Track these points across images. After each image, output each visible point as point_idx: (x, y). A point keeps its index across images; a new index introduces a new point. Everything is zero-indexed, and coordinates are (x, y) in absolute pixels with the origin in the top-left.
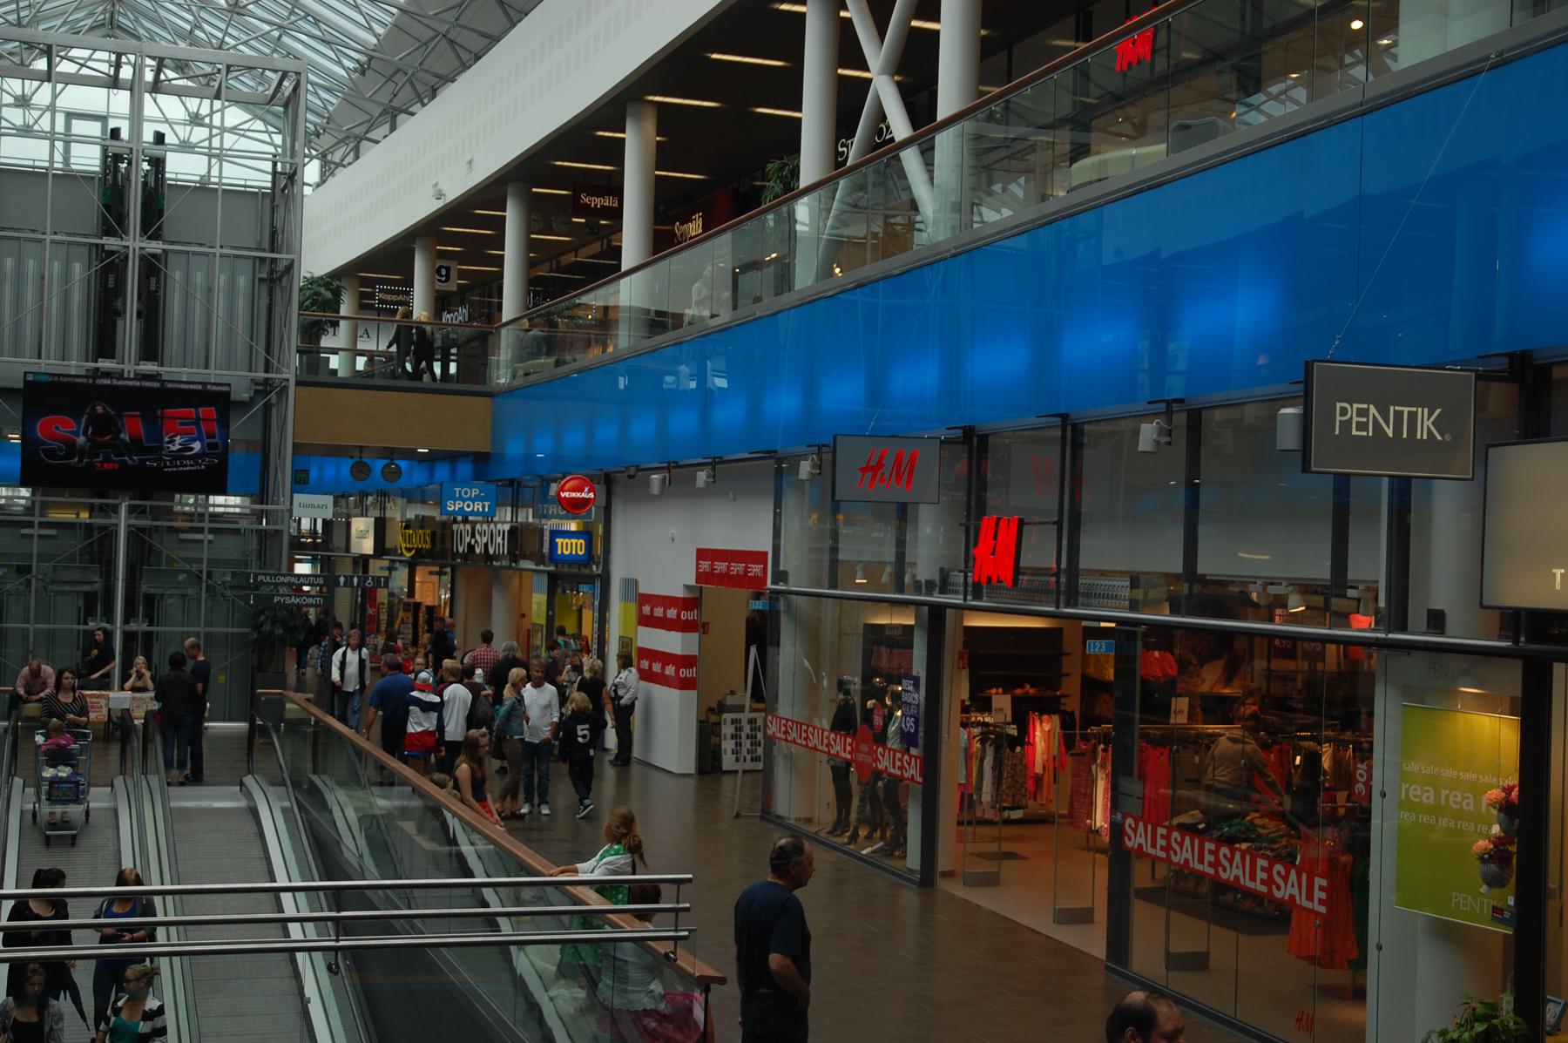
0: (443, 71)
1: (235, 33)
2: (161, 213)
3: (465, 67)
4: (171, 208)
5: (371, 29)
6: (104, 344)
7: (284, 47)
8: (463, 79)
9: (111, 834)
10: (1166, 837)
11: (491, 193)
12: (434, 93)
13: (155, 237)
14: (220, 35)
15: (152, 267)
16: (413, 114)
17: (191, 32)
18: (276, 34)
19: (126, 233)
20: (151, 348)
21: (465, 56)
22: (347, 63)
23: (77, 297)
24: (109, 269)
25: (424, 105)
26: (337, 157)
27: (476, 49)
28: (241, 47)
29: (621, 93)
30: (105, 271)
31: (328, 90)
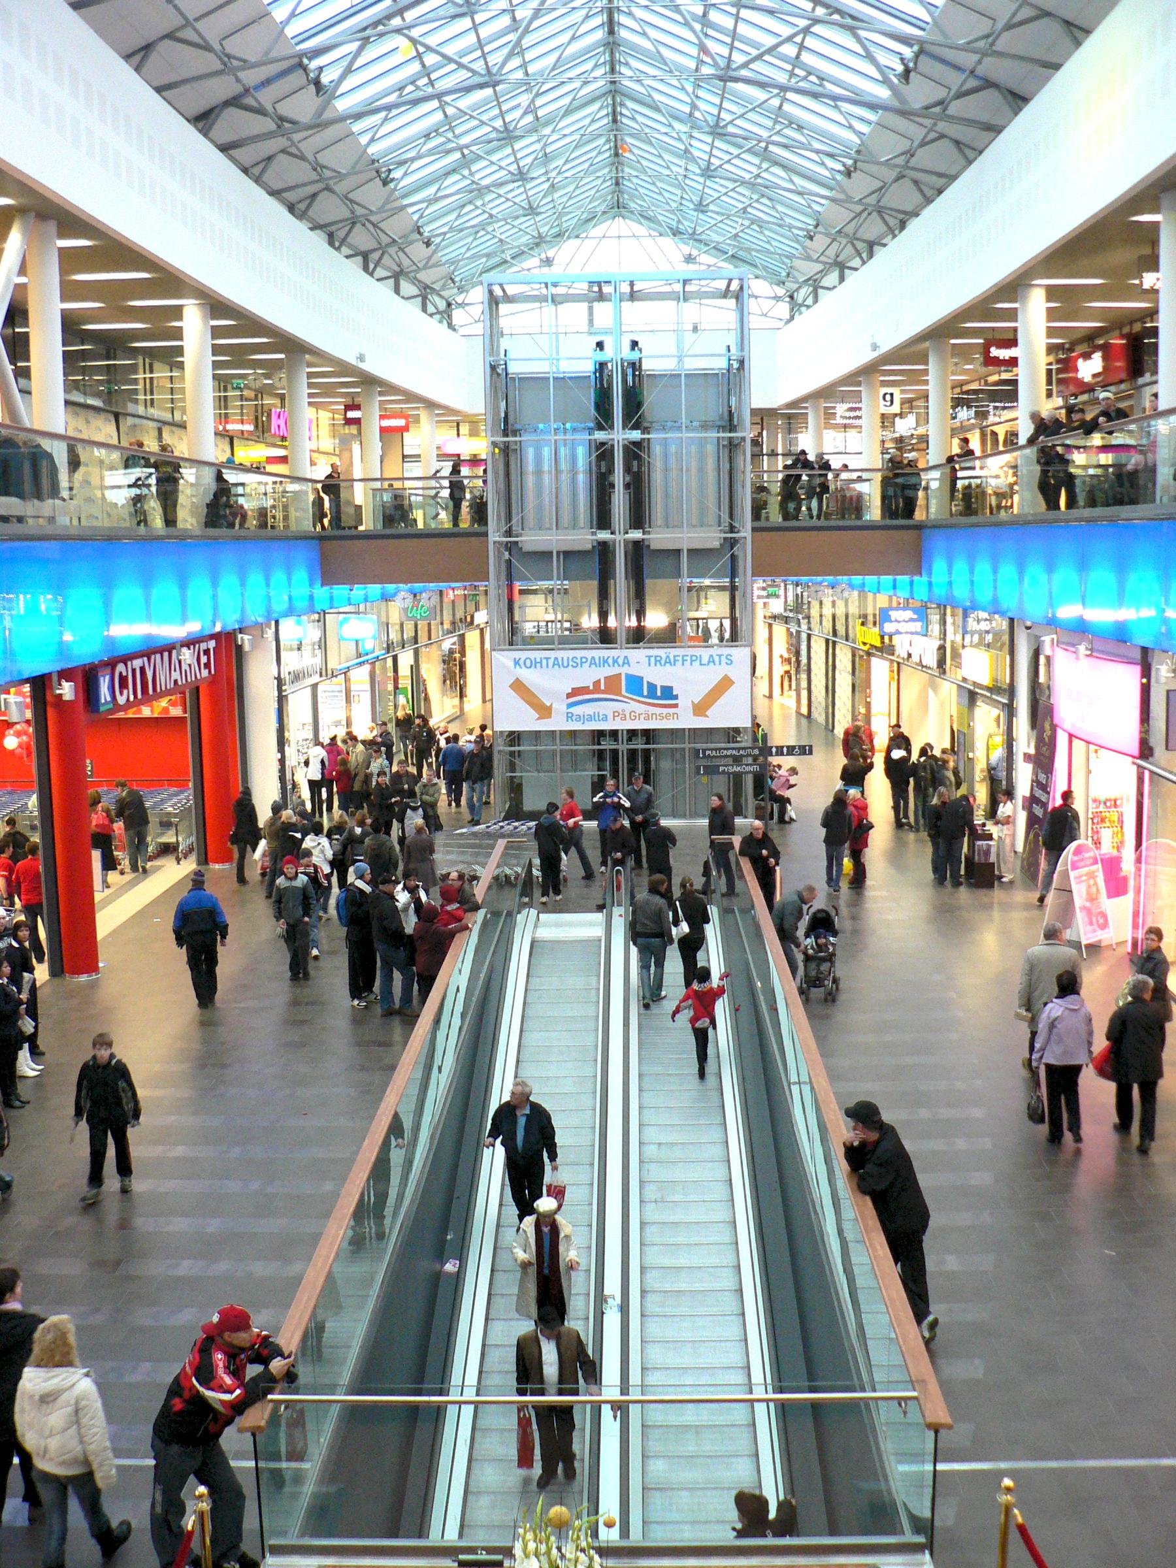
0: (909, 208)
1: (733, 108)
2: (639, 405)
3: (929, 201)
4: (651, 398)
5: (851, 127)
6: (603, 520)
7: (804, 66)
8: (927, 213)
9: (717, 1094)
10: (25, 733)
11: (1013, 287)
12: (903, 225)
13: (636, 427)
14: (700, 187)
15: (634, 452)
16: (885, 245)
17: (691, 115)
18: (776, 102)
19: (612, 427)
20: (638, 519)
21: (929, 192)
22: (883, 59)
23: (581, 478)
24: (603, 453)
25: (895, 236)
26: (825, 282)
27: (938, 185)
28: (726, 166)
29: (1105, 217)
30: (600, 458)
31: (831, 155)
